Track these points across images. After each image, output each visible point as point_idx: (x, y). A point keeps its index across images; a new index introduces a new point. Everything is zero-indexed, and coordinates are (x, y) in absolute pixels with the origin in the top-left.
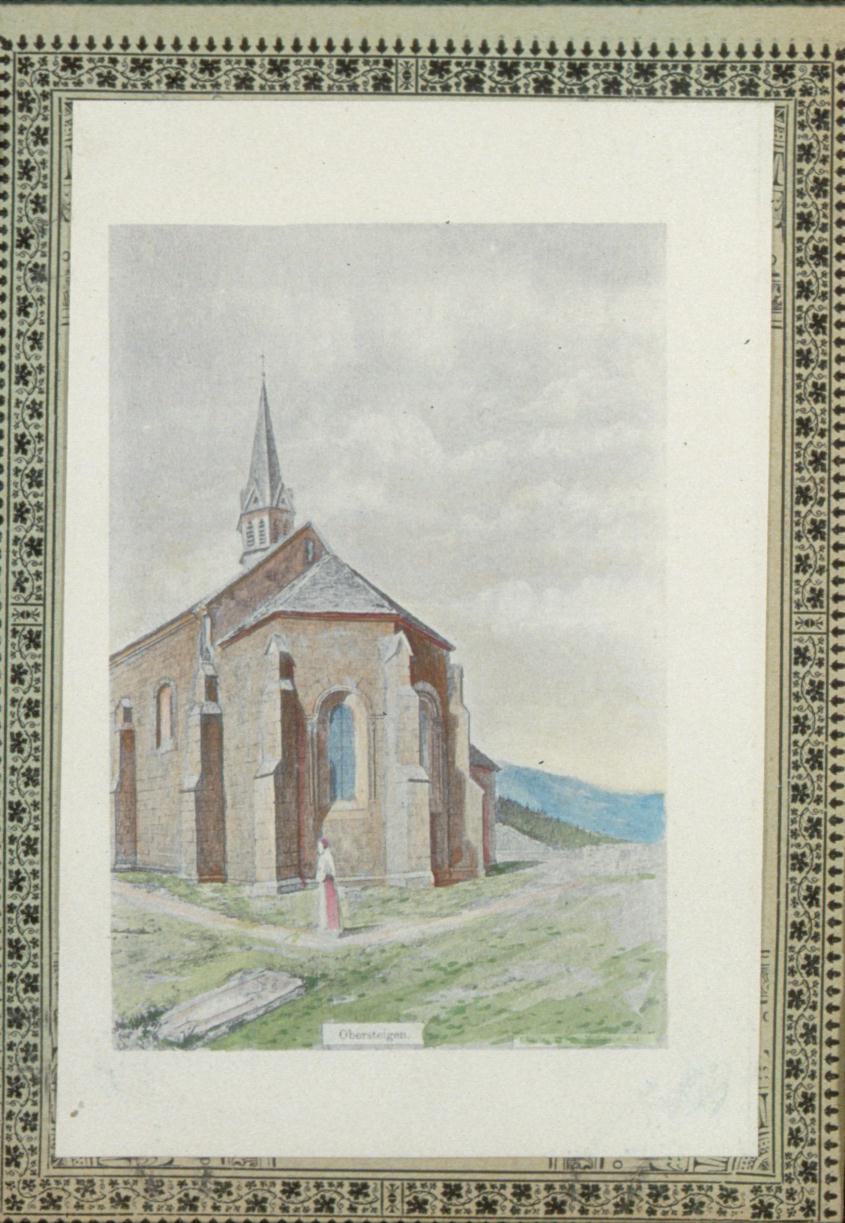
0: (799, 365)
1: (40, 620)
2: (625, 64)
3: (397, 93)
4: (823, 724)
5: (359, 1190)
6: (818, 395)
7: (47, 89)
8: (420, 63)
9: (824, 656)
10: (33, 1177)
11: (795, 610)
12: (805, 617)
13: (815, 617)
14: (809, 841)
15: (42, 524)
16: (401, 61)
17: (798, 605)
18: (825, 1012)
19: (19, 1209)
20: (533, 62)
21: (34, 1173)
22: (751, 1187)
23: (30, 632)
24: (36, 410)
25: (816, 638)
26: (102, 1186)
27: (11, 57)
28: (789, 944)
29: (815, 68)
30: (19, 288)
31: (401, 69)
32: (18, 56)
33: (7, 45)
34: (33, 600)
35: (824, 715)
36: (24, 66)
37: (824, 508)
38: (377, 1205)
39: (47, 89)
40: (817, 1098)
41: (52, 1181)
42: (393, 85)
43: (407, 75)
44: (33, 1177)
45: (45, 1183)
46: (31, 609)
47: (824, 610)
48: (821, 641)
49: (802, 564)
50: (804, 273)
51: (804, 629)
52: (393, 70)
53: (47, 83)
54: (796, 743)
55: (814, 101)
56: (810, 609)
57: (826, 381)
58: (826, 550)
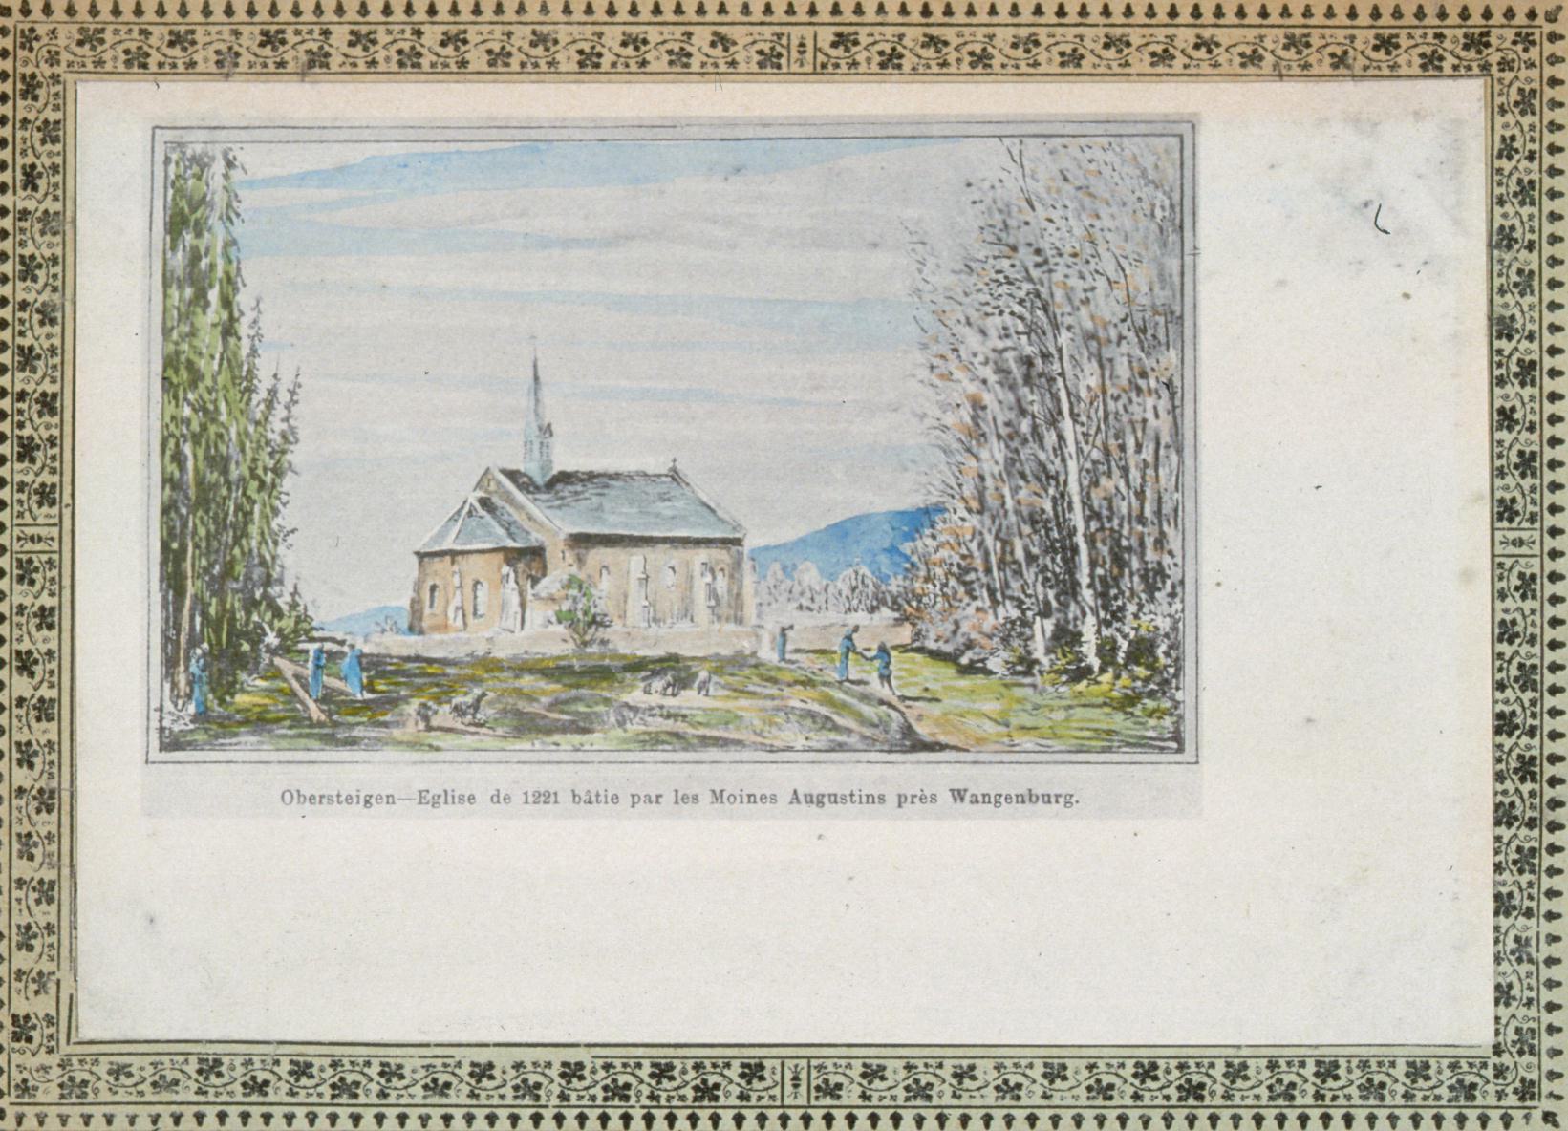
0: (1137, 1065)
1: (795, 68)
2: (1536, 832)
3: (1493, 530)
4: (663, 1102)
5: (46, 495)
6: (1188, 1091)
7: (1494, 69)
8: (1532, 561)
9: (753, 1102)
10: (64, 64)
11: (814, 1062)
12: (803, 1075)
13: (803, 1089)
14: (510, 1084)
15: (921, 70)
16: (1537, 535)
17: (820, 1068)
18: (465, 1110)
19: (23, 46)
20: (1538, 709)
21: (70, 64)
22: (53, 1013)
23: (779, 55)
24: (890, 60)
25: (777, 1091)
26: (50, 154)
27: (1537, 22)
28: (1217, 1062)
29: (1532, 1083)
30: (1410, 36)
31: (1525, 535)
32: (20, 26)
33: (5, 11)
34: (821, 58)
35: (675, 1103)
36: (28, 39)
37: (947, 1100)
38: (28, 519)
39: (1494, 69)
40: (261, 1099)
41: (59, 88)
42: (1505, 524)
43: (1519, 543)
44: (64, 64)
45: (55, 79)
46: (809, 56)
47: (813, 1103)
48: (772, 1097)
49: (873, 1073)
50: (684, 1072)
51: (788, 1075)
52: (1526, 525)
53: (1502, 70)
54: (639, 1066)
55: (1488, 1082)
56: (814, 1083)
57: (935, 1101)
58: (1345, 1103)
